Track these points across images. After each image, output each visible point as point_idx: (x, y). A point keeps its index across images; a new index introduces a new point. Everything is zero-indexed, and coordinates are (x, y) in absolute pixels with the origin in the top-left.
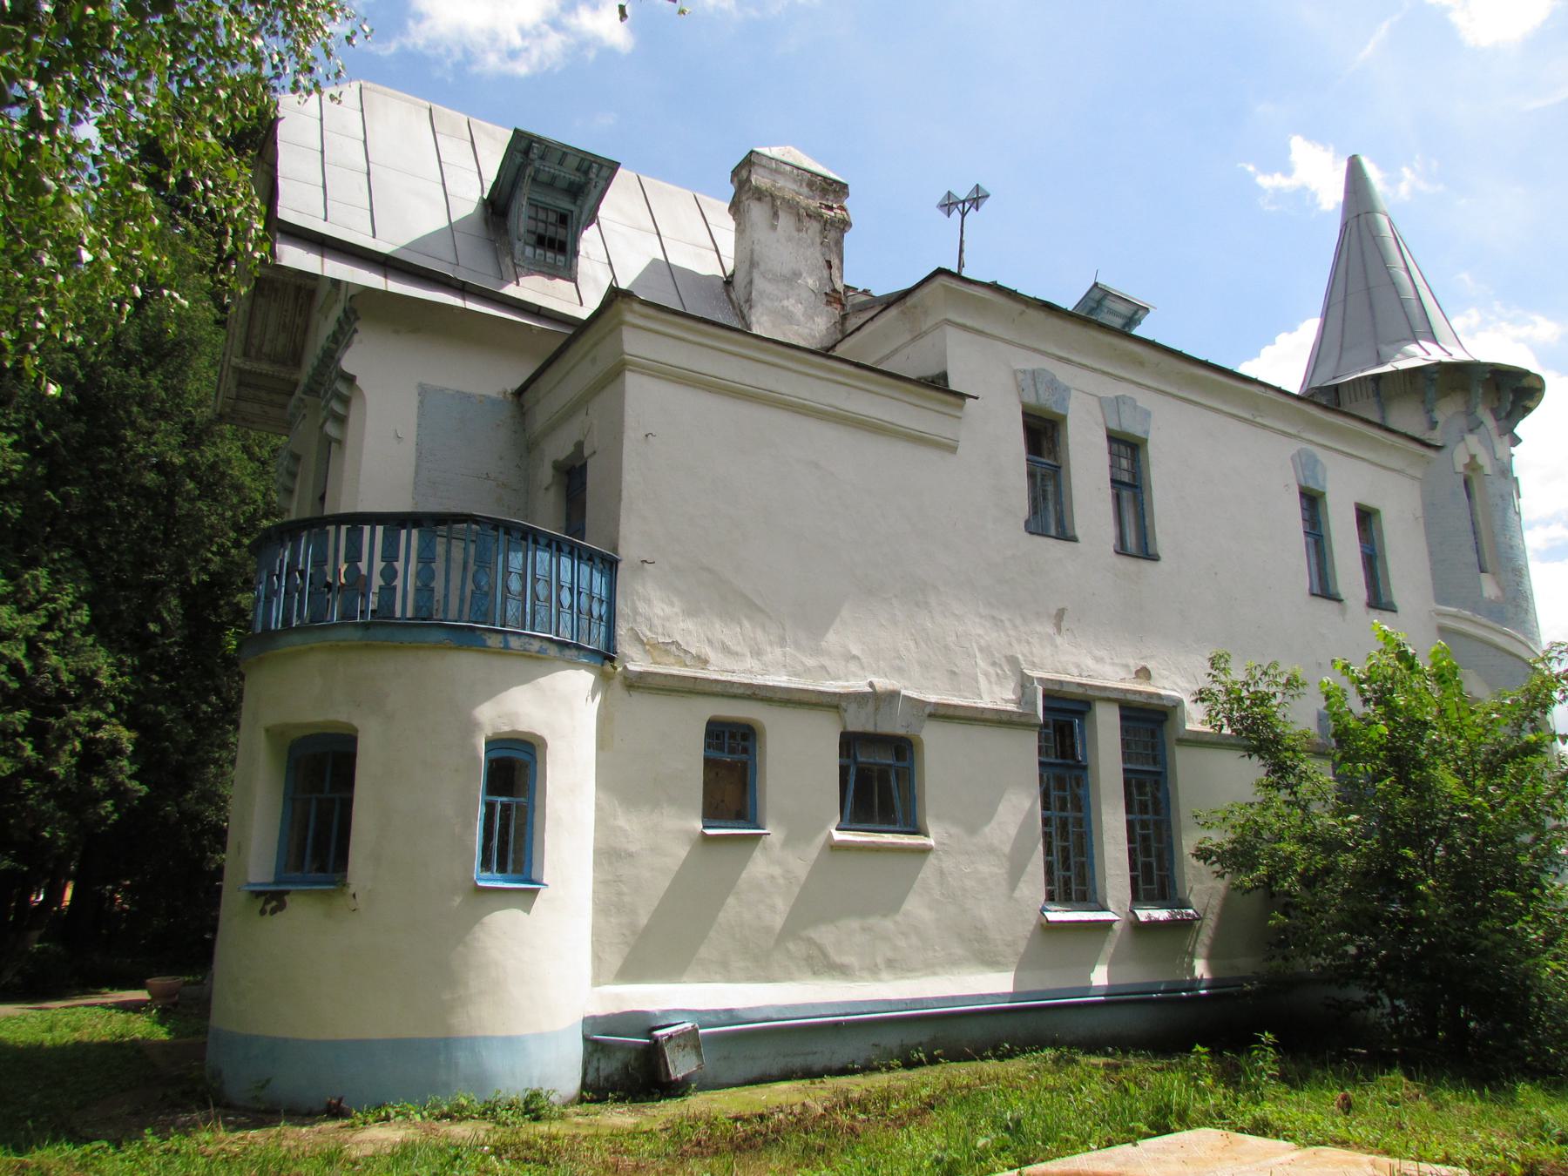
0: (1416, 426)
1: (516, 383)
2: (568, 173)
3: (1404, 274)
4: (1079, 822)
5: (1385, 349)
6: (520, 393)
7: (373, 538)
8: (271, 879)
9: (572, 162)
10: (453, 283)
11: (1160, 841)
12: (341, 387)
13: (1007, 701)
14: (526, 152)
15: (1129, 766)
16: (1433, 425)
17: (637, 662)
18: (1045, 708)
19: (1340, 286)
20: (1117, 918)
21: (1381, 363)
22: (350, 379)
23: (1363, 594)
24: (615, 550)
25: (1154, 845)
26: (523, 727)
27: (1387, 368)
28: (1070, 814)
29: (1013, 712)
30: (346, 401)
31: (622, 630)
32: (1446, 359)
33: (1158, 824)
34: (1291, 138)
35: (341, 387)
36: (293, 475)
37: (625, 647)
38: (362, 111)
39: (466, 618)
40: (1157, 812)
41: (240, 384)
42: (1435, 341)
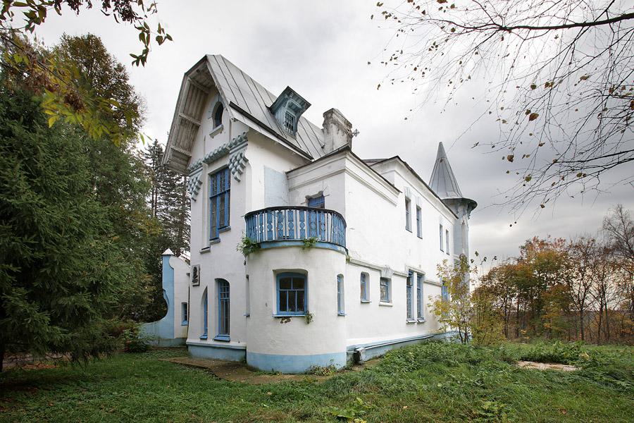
22: (246, 161)
30: (243, 167)
36: (199, 189)
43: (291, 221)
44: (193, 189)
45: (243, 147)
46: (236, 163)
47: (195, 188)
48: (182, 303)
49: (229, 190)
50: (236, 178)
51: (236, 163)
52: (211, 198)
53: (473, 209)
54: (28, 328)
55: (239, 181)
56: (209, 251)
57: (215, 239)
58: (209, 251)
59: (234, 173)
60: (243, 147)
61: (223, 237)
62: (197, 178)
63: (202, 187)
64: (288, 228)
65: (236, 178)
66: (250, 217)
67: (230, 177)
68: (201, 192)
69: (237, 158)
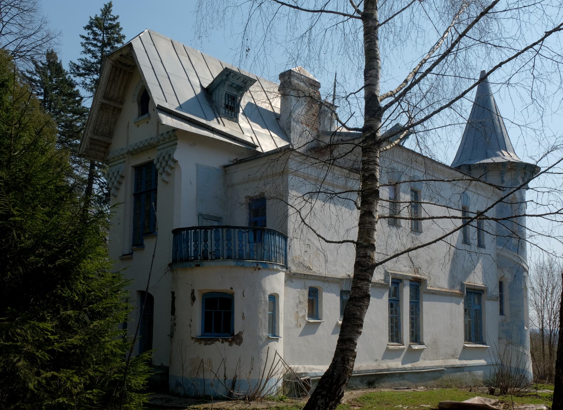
0: (497, 182)
1: (226, 163)
2: (239, 83)
3: (498, 122)
4: (396, 318)
5: (489, 152)
6: (225, 167)
7: (235, 233)
8: (200, 334)
9: (242, 79)
10: (210, 128)
11: (416, 324)
12: (172, 164)
13: (381, 280)
14: (227, 75)
15: (412, 301)
16: (503, 182)
17: (294, 269)
18: (392, 282)
19: (472, 115)
20: (426, 347)
21: (487, 157)
22: (175, 162)
23: (476, 242)
24: (287, 234)
25: (415, 325)
26: (275, 292)
27: (489, 161)
28: (395, 315)
29: (383, 284)
30: (172, 168)
31: (289, 258)
32: (512, 160)
33: (416, 319)
34: (525, 193)
35: (172, 164)
36: (120, 183)
37: (290, 264)
38: (154, 45)
39: (259, 258)
40: (396, 314)
41: (91, 144)
42: (506, 151)
43: (229, 239)
44: (113, 184)
45: (172, 146)
46: (164, 164)
47: (115, 183)
48: (138, 291)
49: (156, 189)
50: (164, 181)
51: (164, 164)
52: (133, 194)
53: (367, 308)
54: (100, 204)
55: (167, 183)
56: (131, 258)
57: (138, 244)
58: (131, 258)
59: (161, 174)
60: (172, 146)
61: (148, 243)
62: (118, 172)
63: (124, 182)
64: (226, 248)
65: (164, 181)
66: (177, 232)
67: (156, 180)
68: (123, 187)
69: (160, 160)
